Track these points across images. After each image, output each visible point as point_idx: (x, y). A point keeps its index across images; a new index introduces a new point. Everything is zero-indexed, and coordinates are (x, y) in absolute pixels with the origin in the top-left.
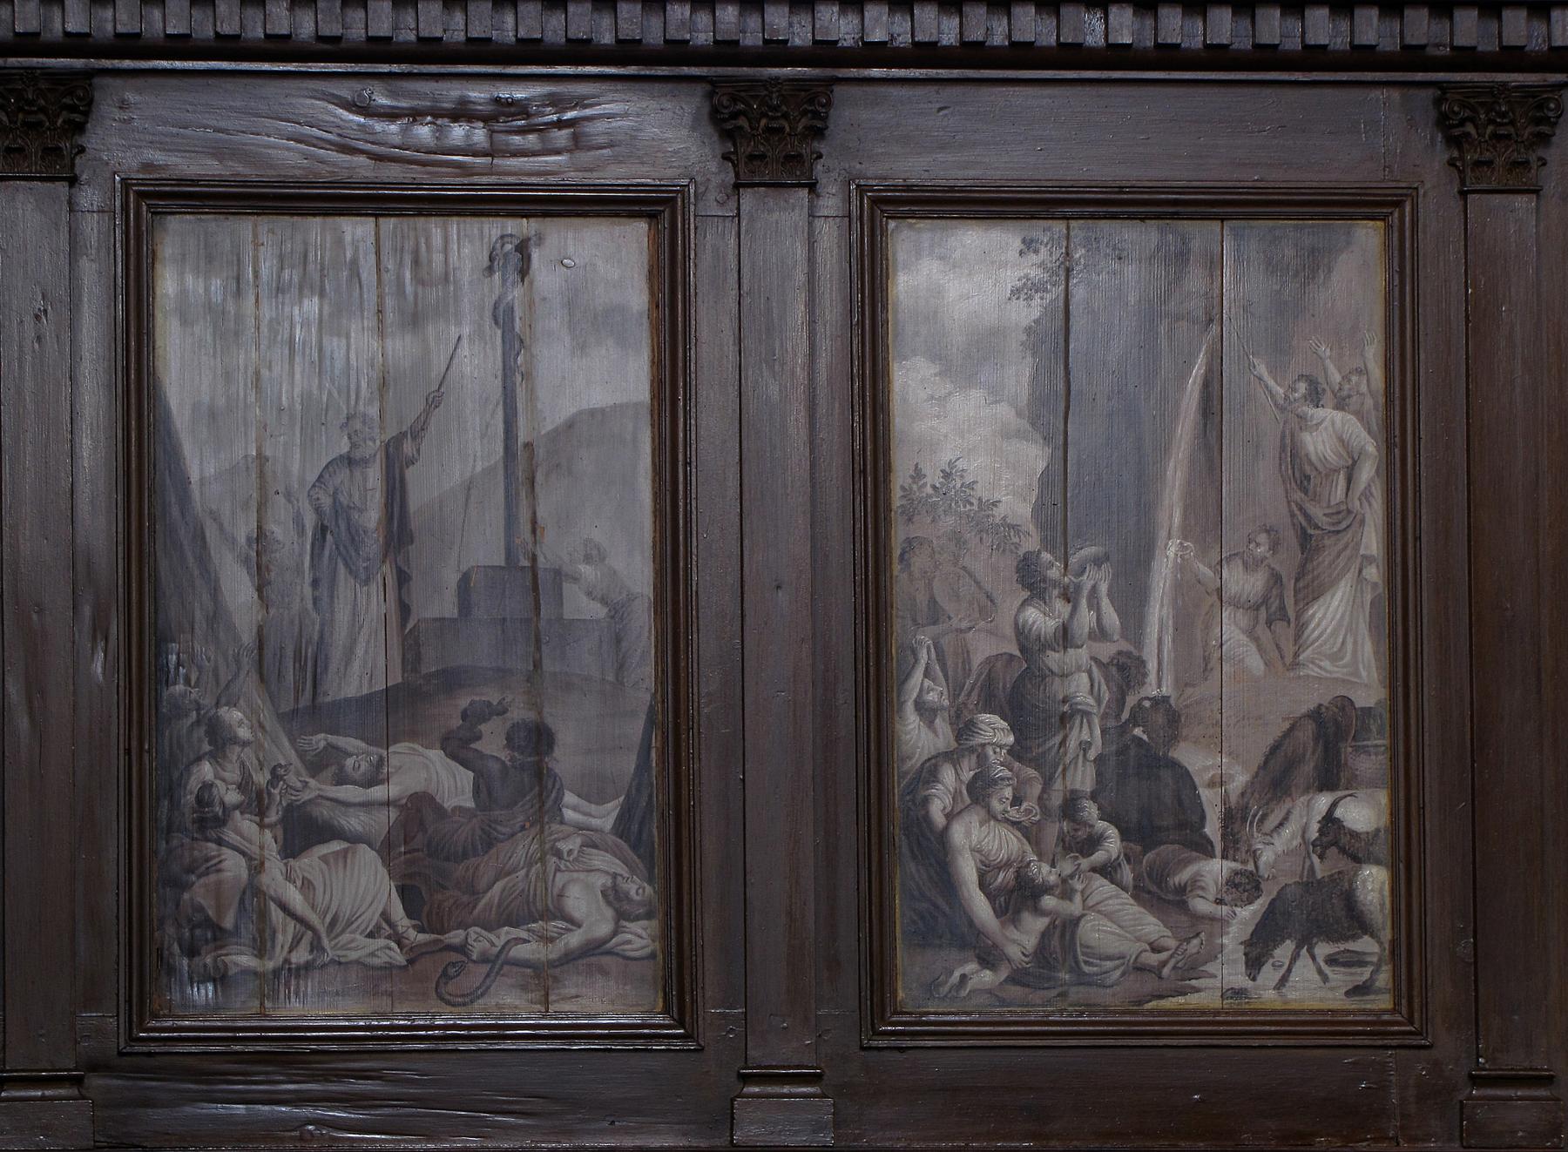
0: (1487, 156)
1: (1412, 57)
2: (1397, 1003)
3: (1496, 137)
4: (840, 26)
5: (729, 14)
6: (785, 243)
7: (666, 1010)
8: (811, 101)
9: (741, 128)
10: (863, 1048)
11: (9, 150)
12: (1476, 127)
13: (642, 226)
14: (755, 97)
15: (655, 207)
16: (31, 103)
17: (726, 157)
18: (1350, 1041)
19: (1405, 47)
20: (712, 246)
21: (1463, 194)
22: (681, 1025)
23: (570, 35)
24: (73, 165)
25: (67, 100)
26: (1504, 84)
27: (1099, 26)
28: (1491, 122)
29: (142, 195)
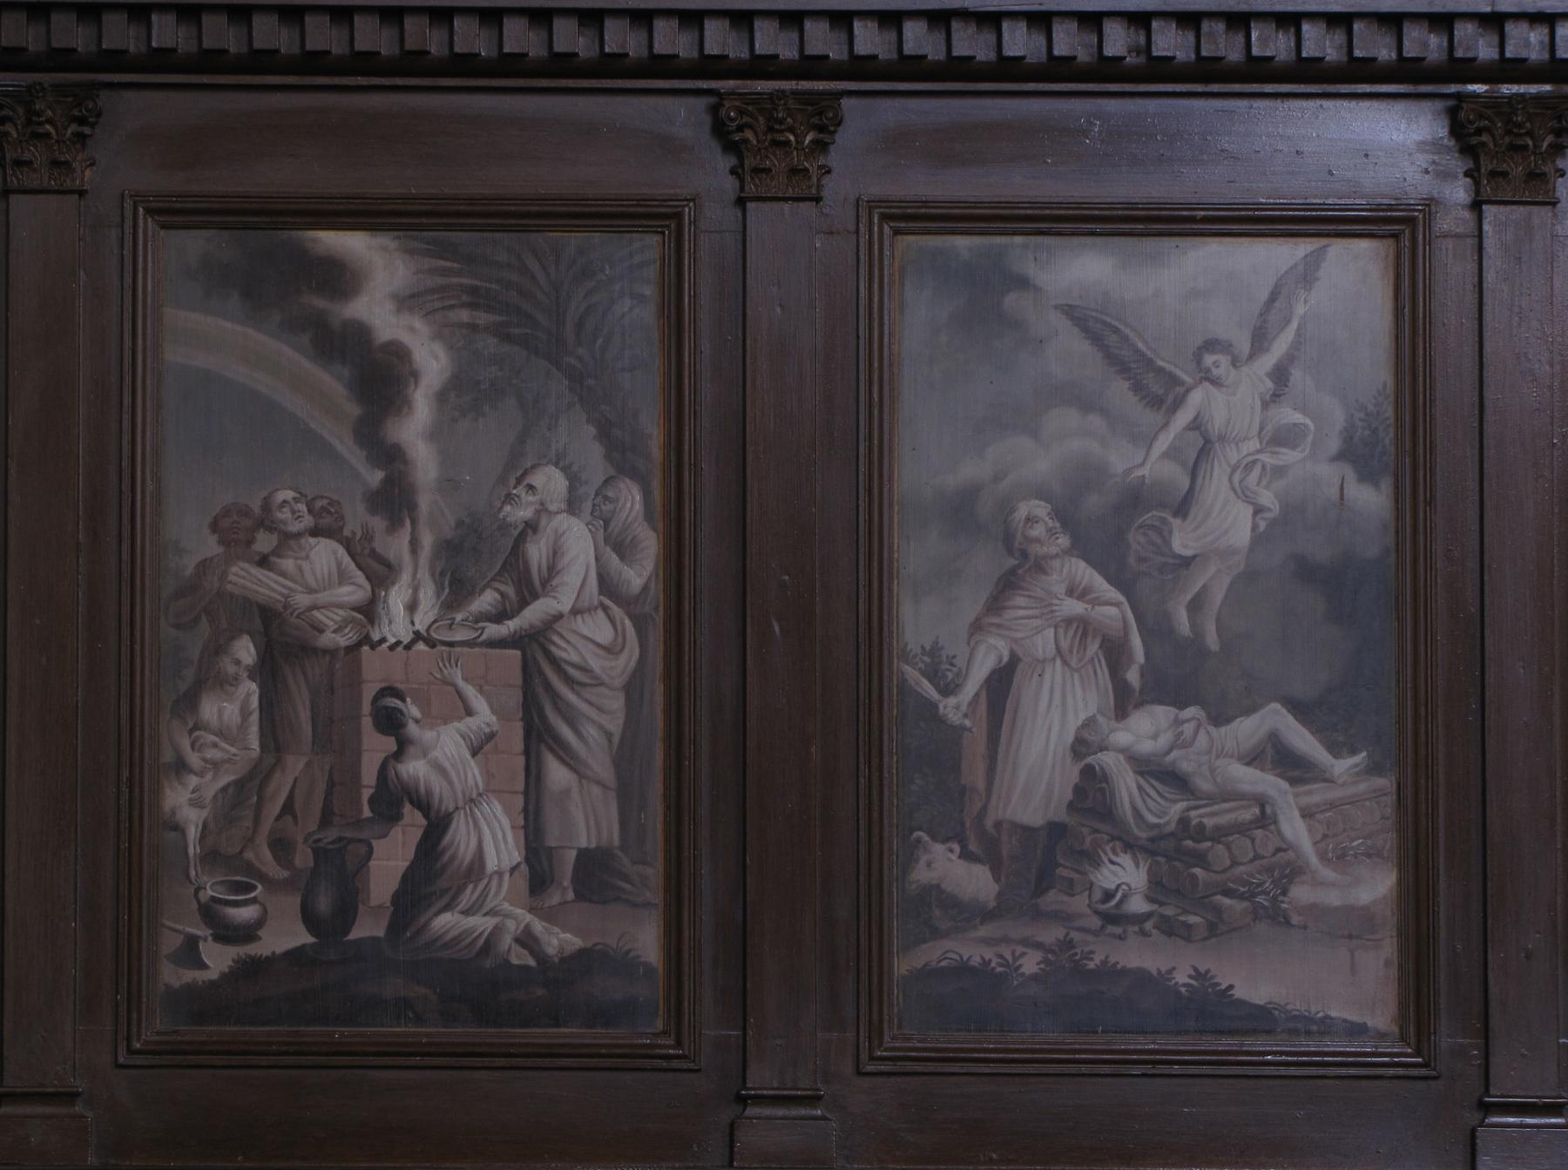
16: (1520, 126)
17: (733, 172)
22: (1418, 1053)
25: (815, 120)
28: (1508, 132)
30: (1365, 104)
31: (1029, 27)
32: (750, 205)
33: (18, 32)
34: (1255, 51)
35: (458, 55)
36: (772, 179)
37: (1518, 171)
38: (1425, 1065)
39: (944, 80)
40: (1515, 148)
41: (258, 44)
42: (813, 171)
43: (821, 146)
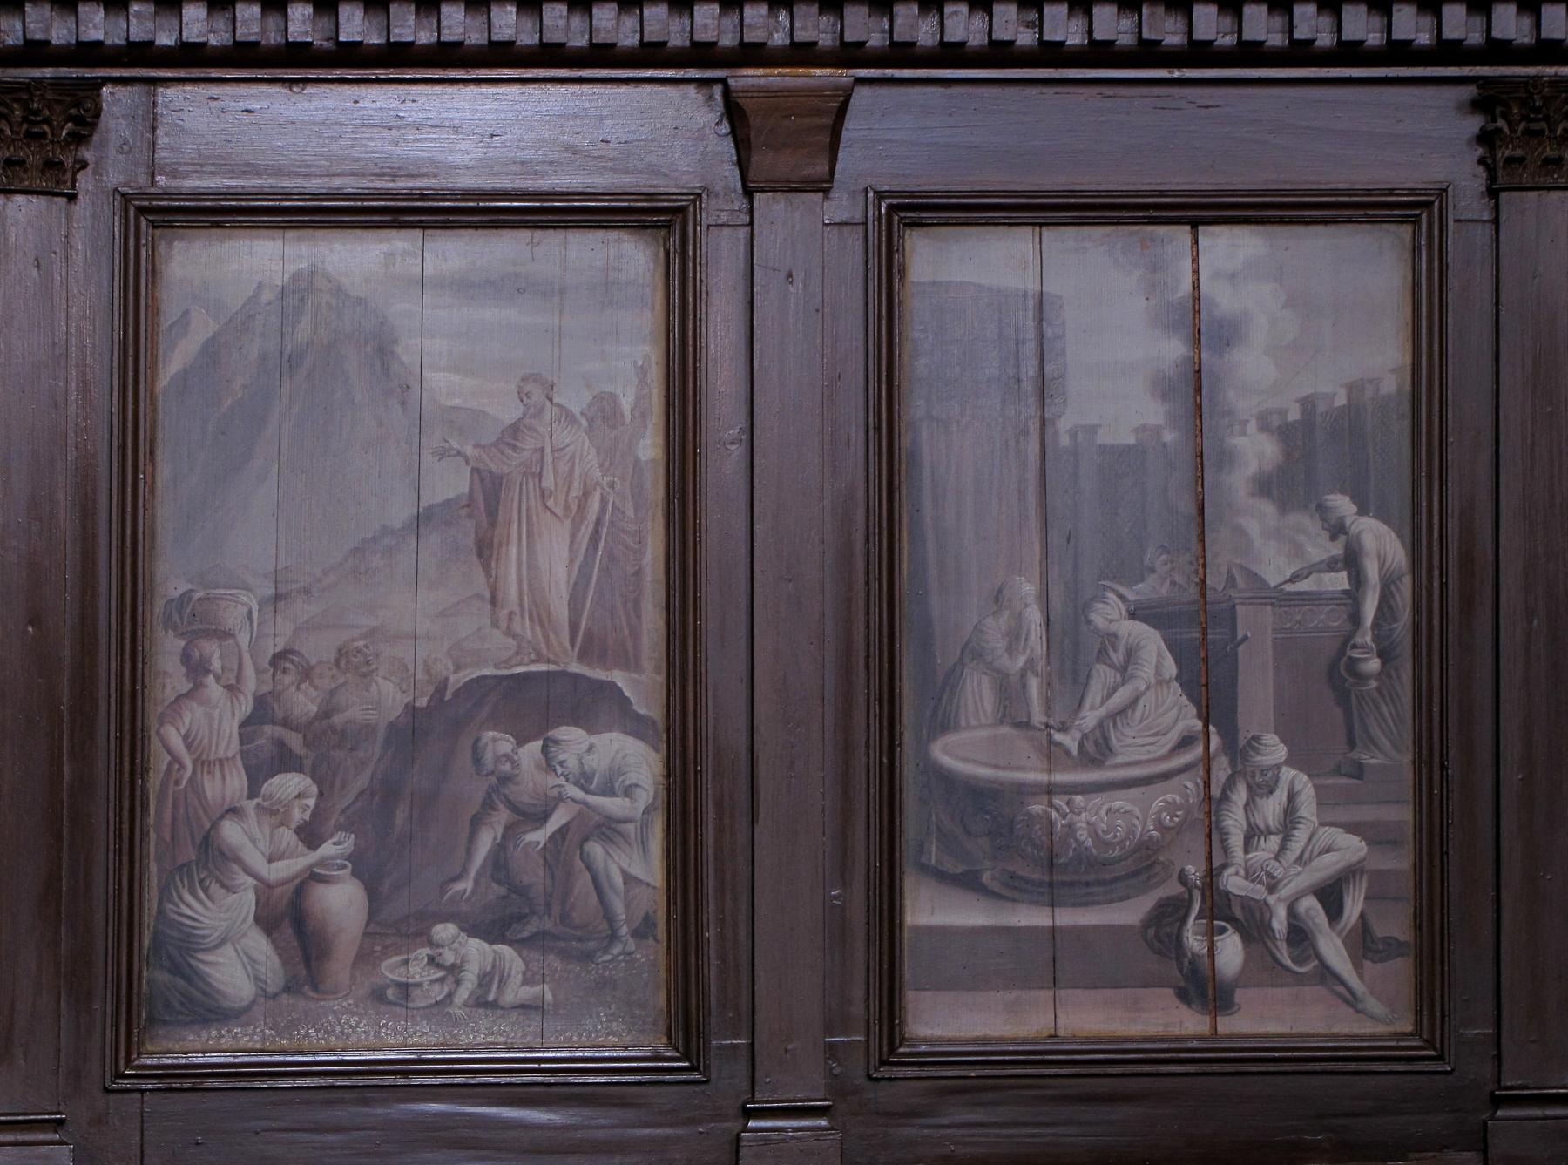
0: (1519, 153)
1: (701, 54)
2: (1418, 1023)
3: (1528, 133)
4: (96, 25)
5: (656, 15)
6: (797, 251)
7: (670, 1043)
8: (78, 105)
9: (1499, 130)
10: (107, 1090)
11: (9, 163)
12: (1509, 124)
13: (1406, 231)
14: (17, 100)
15: (1414, 210)
16: (37, 113)
17: (1481, 161)
18: (1317, 1067)
19: (694, 44)
20: (722, 256)
21: (749, 193)
22: (685, 1057)
23: (697, 38)
24: (74, 181)
25: (73, 111)
26: (1538, 77)
27: (18, 25)
28: (1524, 118)
29: (142, 211)
30: (438, 89)
31: (1369, 12)
32: (1503, 195)
33: (6, 30)
34: (1145, 35)
35: (134, 43)
36: (26, 171)
37: (34, 159)
38: (1440, 1058)
39: (1180, 66)
40: (32, 136)
41: (1098, 35)
42: (69, 162)
43: (79, 139)
